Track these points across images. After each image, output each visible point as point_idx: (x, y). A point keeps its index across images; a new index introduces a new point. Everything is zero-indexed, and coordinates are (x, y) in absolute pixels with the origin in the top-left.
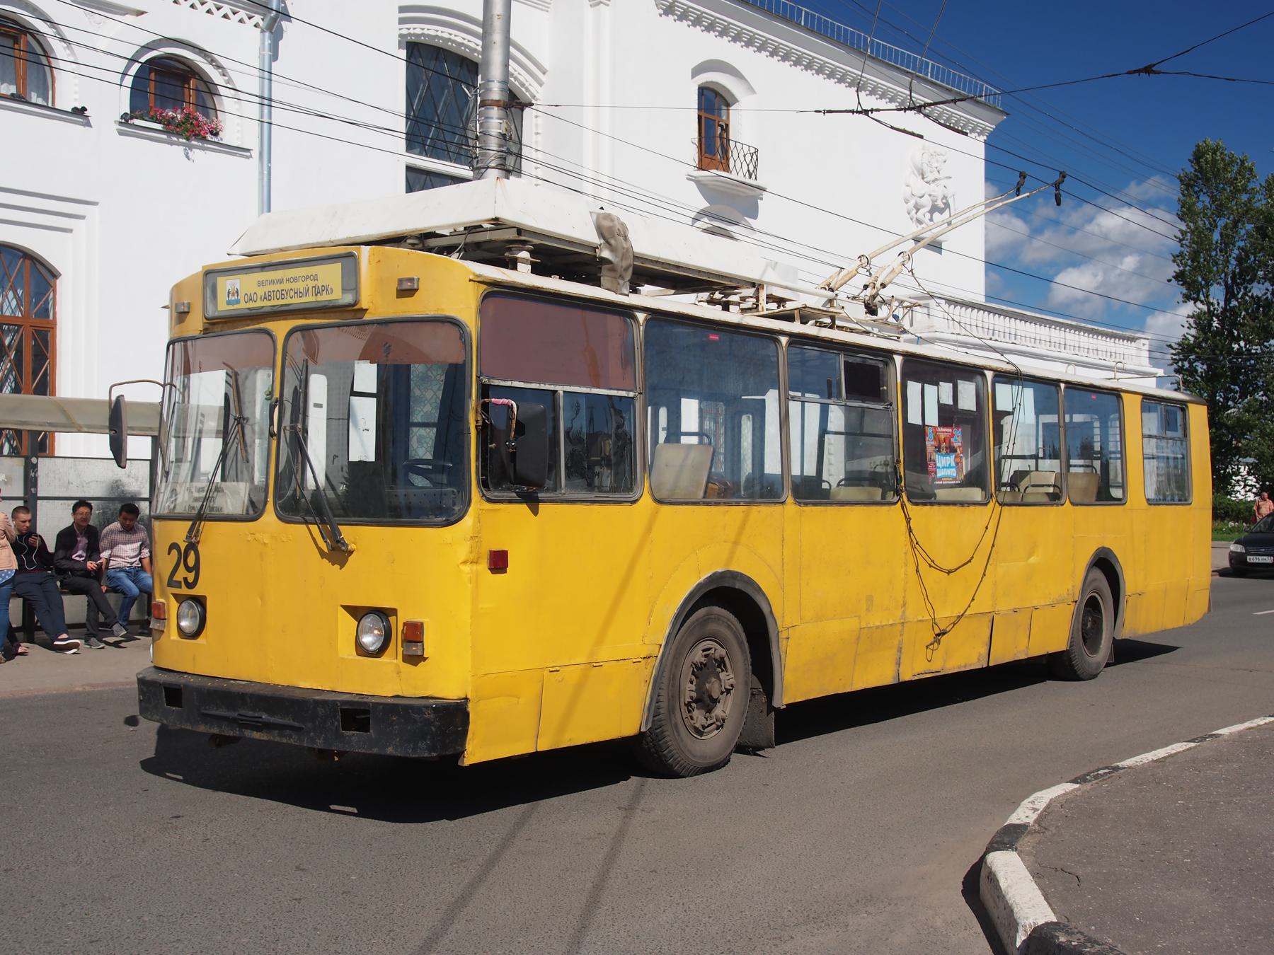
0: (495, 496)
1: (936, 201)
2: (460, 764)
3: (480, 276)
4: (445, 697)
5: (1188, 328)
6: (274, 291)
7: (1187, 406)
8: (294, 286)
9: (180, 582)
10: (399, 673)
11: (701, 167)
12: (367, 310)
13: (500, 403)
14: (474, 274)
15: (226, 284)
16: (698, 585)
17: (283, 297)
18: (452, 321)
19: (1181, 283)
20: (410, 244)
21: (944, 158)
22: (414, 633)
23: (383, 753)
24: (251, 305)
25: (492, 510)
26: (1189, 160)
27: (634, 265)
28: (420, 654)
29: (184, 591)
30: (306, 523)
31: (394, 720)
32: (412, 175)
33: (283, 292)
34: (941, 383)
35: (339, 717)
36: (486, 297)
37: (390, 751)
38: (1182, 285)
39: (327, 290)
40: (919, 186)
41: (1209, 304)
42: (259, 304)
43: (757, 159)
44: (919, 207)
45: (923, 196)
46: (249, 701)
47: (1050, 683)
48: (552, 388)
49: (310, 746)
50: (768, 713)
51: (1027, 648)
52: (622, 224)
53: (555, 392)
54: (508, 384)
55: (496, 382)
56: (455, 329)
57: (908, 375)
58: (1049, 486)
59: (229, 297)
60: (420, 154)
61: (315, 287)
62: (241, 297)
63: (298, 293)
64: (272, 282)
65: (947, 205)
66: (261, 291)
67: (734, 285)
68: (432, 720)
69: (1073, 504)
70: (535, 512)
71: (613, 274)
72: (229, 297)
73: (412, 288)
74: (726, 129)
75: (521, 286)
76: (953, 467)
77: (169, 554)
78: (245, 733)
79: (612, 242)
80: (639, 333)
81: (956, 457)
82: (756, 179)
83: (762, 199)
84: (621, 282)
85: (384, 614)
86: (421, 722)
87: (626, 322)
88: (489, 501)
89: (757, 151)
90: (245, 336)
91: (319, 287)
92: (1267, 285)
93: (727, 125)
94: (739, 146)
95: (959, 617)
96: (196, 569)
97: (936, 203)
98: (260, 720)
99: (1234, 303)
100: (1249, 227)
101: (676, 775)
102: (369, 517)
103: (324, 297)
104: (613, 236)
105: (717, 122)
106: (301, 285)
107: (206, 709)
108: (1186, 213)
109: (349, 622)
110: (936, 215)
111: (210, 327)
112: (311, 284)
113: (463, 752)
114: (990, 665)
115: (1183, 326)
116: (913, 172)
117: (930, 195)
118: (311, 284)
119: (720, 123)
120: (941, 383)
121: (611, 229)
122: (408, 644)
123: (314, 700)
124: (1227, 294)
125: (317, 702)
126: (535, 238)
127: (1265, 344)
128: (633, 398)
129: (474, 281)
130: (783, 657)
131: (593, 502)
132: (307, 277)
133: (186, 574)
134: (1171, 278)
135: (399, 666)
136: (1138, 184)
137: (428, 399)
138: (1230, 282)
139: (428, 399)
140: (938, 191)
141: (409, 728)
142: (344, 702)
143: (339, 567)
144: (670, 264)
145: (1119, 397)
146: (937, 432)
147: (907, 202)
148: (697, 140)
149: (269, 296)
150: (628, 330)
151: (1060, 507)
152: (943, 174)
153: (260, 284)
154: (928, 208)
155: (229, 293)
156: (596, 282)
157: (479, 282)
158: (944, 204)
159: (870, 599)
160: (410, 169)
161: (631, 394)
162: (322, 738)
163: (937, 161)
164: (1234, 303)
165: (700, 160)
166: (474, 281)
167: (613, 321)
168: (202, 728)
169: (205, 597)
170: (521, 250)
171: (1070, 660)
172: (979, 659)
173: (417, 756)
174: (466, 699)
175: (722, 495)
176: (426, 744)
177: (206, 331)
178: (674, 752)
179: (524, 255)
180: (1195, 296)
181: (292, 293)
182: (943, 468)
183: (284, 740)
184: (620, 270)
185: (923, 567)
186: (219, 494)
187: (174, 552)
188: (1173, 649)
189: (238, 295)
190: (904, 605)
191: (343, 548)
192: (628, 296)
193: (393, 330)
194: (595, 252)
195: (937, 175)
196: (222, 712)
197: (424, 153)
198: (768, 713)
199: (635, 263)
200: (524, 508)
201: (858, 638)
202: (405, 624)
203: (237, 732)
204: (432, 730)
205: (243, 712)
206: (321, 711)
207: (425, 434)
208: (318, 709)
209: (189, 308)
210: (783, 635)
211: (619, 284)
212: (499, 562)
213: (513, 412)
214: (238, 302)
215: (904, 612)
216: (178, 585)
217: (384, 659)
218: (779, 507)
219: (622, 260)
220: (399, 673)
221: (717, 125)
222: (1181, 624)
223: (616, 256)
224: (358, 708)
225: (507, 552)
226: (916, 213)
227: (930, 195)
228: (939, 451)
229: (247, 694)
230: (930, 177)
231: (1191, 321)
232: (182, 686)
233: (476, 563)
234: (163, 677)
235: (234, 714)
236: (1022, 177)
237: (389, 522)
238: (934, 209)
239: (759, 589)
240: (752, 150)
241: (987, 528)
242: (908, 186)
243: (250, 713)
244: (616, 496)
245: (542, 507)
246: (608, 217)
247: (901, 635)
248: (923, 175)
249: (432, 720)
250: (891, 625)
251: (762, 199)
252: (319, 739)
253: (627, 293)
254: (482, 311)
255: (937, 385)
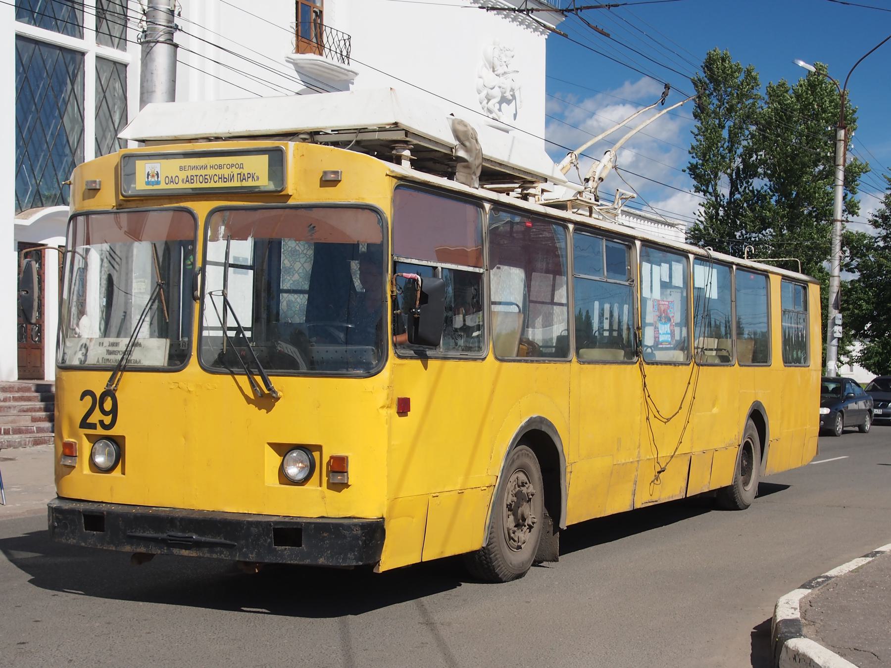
0: (403, 354)
1: (505, 93)
2: (375, 571)
3: (393, 172)
4: (365, 517)
5: (699, 216)
6: (197, 176)
7: (808, 285)
8: (219, 172)
9: (96, 424)
10: (323, 498)
11: (298, 50)
12: (291, 195)
13: (410, 277)
14: (389, 170)
15: (143, 168)
16: (521, 427)
17: (206, 181)
18: (372, 208)
19: (693, 176)
20: (302, 139)
21: (512, 54)
22: (339, 466)
23: (314, 563)
24: (172, 186)
25: (400, 364)
26: (702, 66)
27: (482, 165)
28: (346, 482)
29: (100, 431)
30: (232, 373)
31: (325, 537)
32: (21, 43)
33: (206, 177)
34: (662, 264)
35: (272, 535)
36: (397, 187)
37: (322, 561)
38: (693, 178)
39: (253, 177)
40: (490, 78)
41: (717, 196)
42: (181, 185)
43: (350, 45)
44: (490, 98)
45: (494, 88)
46: (178, 524)
47: (713, 513)
48: (434, 264)
49: (242, 559)
50: (554, 533)
51: (709, 483)
52: (473, 129)
53: (435, 268)
54: (408, 261)
55: (402, 260)
56: (374, 214)
57: (646, 257)
58: (711, 350)
59: (148, 178)
60: (29, 23)
61: (240, 174)
62: (162, 178)
63: (222, 178)
64: (195, 168)
65: (514, 96)
66: (183, 175)
67: (533, 180)
68: (359, 536)
69: (740, 365)
70: (426, 367)
71: (466, 170)
72: (148, 178)
73: (336, 179)
74: (319, 15)
75: (417, 180)
76: (668, 334)
77: (81, 399)
78: (174, 551)
79: (467, 144)
80: (486, 219)
81: (670, 325)
82: (348, 63)
83: (353, 83)
84: (474, 177)
85: (307, 449)
86: (350, 537)
87: (477, 210)
88: (399, 357)
89: (349, 38)
90: (164, 213)
91: (244, 174)
92: (766, 180)
93: (321, 12)
94: (334, 32)
95: (672, 457)
96: (114, 412)
97: (505, 95)
98: (192, 540)
99: (737, 196)
100: (753, 128)
101: (500, 581)
102: (238, 368)
103: (250, 183)
104: (468, 139)
105: (312, 8)
106: (226, 172)
107: (132, 532)
108: (700, 111)
109: (273, 460)
110: (504, 105)
111: (125, 203)
112: (236, 171)
113: (379, 561)
114: (688, 496)
115: (695, 214)
116: (485, 64)
117: (500, 87)
118: (236, 171)
119: (315, 9)
120: (662, 264)
121: (466, 133)
122: (334, 474)
123: (248, 522)
124: (732, 188)
125: (250, 524)
126: (416, 140)
127: (764, 232)
128: (482, 274)
129: (390, 176)
130: (567, 487)
131: (460, 359)
132: (232, 166)
133: (101, 416)
134: (686, 169)
135: (324, 492)
136: (632, 83)
137: (297, 270)
138: (734, 177)
139: (297, 270)
140: (506, 83)
141: (339, 542)
142: (276, 523)
143: (265, 411)
144: (496, 162)
145: (767, 277)
146: (659, 304)
147: (479, 92)
148: (295, 24)
149: (191, 179)
150: (478, 218)
151: (732, 368)
152: (510, 69)
153: (182, 168)
154: (498, 99)
155: (148, 175)
156: (451, 176)
157: (393, 177)
158: (512, 96)
159: (619, 441)
160: (19, 37)
161: (481, 271)
162: (254, 553)
163: (506, 56)
164: (737, 196)
165: (297, 46)
166: (390, 176)
167: (470, 209)
168: (128, 548)
169: (123, 437)
170: (405, 149)
171: (733, 494)
172: (680, 492)
173: (347, 565)
174: (383, 518)
175: (530, 354)
176: (354, 555)
177: (120, 206)
178: (500, 563)
179: (407, 153)
180: (704, 188)
181: (216, 178)
182: (663, 334)
183: (215, 556)
184: (474, 167)
185: (651, 416)
186: (136, 348)
187: (88, 399)
188: (785, 487)
189: (158, 177)
190: (639, 446)
191: (274, 395)
192: (477, 189)
193: (315, 213)
194: (452, 152)
195: (506, 69)
196: (150, 534)
197: (33, 22)
198: (554, 533)
199: (483, 164)
200: (419, 363)
201: (612, 473)
202: (331, 457)
203: (165, 551)
204: (359, 543)
205: (172, 533)
206: (254, 530)
207: (294, 300)
208: (252, 528)
209: (100, 185)
210: (568, 470)
211: (472, 179)
212: (403, 407)
213: (418, 284)
214: (158, 183)
215: (639, 452)
216: (93, 426)
217: (308, 487)
218: (568, 365)
219: (475, 159)
220: (323, 498)
221: (312, 11)
222: (800, 465)
223: (470, 156)
224: (291, 527)
225: (409, 399)
226: (487, 103)
227: (500, 87)
228: (661, 320)
229: (176, 518)
230: (500, 70)
231: (702, 209)
232: (105, 513)
233: (390, 407)
234: (67, 506)
235: (165, 536)
236: (667, 89)
237: (321, 374)
238: (504, 100)
239: (556, 432)
240: (346, 37)
241: (689, 383)
242: (480, 78)
243: (180, 534)
244: (473, 354)
245: (431, 363)
246: (461, 122)
247: (637, 470)
248: (493, 68)
249: (359, 536)
250: (631, 462)
251: (353, 83)
252: (252, 554)
253: (477, 186)
254: (394, 201)
255: (660, 265)
